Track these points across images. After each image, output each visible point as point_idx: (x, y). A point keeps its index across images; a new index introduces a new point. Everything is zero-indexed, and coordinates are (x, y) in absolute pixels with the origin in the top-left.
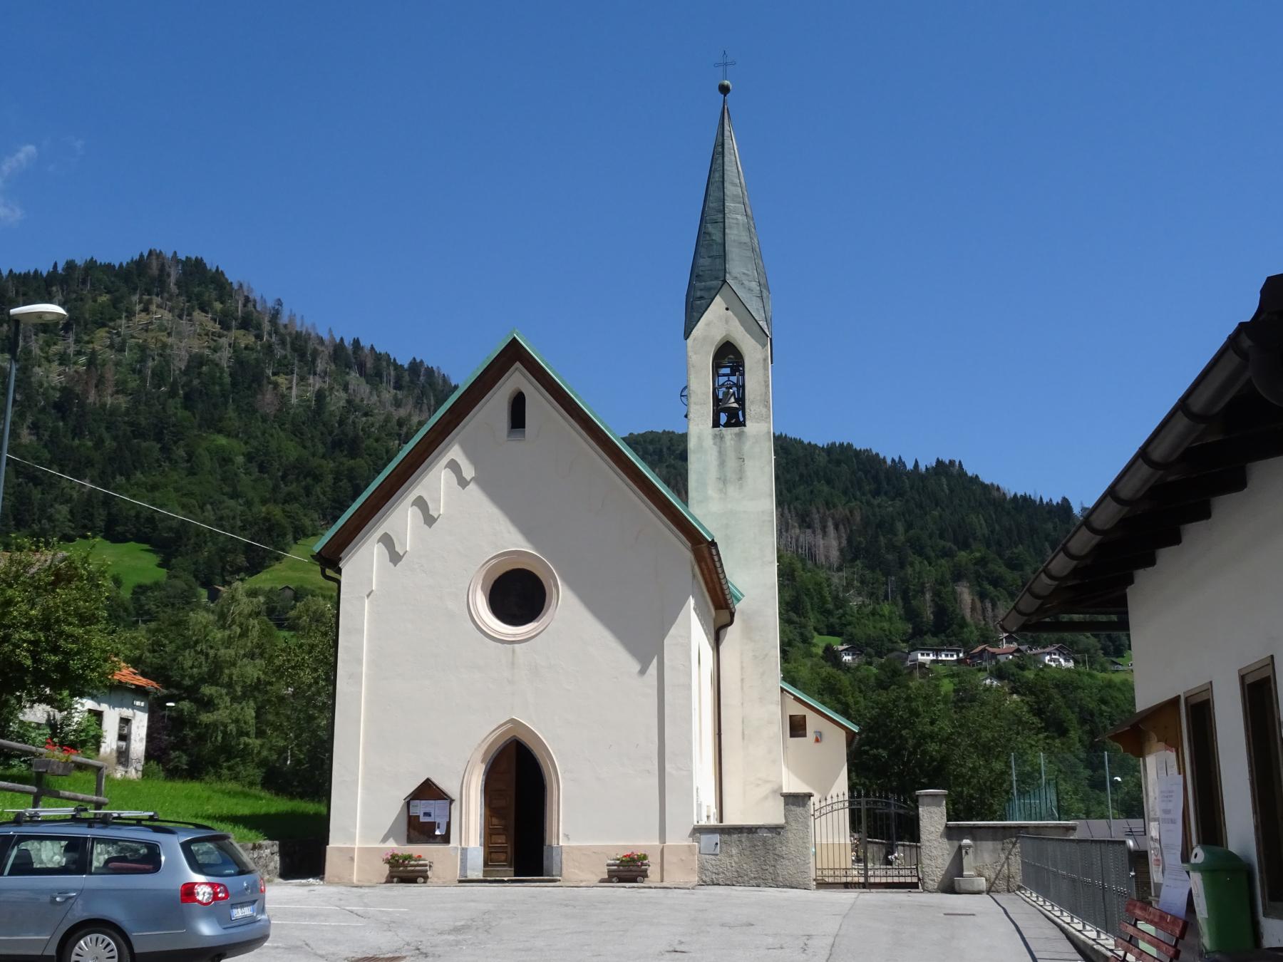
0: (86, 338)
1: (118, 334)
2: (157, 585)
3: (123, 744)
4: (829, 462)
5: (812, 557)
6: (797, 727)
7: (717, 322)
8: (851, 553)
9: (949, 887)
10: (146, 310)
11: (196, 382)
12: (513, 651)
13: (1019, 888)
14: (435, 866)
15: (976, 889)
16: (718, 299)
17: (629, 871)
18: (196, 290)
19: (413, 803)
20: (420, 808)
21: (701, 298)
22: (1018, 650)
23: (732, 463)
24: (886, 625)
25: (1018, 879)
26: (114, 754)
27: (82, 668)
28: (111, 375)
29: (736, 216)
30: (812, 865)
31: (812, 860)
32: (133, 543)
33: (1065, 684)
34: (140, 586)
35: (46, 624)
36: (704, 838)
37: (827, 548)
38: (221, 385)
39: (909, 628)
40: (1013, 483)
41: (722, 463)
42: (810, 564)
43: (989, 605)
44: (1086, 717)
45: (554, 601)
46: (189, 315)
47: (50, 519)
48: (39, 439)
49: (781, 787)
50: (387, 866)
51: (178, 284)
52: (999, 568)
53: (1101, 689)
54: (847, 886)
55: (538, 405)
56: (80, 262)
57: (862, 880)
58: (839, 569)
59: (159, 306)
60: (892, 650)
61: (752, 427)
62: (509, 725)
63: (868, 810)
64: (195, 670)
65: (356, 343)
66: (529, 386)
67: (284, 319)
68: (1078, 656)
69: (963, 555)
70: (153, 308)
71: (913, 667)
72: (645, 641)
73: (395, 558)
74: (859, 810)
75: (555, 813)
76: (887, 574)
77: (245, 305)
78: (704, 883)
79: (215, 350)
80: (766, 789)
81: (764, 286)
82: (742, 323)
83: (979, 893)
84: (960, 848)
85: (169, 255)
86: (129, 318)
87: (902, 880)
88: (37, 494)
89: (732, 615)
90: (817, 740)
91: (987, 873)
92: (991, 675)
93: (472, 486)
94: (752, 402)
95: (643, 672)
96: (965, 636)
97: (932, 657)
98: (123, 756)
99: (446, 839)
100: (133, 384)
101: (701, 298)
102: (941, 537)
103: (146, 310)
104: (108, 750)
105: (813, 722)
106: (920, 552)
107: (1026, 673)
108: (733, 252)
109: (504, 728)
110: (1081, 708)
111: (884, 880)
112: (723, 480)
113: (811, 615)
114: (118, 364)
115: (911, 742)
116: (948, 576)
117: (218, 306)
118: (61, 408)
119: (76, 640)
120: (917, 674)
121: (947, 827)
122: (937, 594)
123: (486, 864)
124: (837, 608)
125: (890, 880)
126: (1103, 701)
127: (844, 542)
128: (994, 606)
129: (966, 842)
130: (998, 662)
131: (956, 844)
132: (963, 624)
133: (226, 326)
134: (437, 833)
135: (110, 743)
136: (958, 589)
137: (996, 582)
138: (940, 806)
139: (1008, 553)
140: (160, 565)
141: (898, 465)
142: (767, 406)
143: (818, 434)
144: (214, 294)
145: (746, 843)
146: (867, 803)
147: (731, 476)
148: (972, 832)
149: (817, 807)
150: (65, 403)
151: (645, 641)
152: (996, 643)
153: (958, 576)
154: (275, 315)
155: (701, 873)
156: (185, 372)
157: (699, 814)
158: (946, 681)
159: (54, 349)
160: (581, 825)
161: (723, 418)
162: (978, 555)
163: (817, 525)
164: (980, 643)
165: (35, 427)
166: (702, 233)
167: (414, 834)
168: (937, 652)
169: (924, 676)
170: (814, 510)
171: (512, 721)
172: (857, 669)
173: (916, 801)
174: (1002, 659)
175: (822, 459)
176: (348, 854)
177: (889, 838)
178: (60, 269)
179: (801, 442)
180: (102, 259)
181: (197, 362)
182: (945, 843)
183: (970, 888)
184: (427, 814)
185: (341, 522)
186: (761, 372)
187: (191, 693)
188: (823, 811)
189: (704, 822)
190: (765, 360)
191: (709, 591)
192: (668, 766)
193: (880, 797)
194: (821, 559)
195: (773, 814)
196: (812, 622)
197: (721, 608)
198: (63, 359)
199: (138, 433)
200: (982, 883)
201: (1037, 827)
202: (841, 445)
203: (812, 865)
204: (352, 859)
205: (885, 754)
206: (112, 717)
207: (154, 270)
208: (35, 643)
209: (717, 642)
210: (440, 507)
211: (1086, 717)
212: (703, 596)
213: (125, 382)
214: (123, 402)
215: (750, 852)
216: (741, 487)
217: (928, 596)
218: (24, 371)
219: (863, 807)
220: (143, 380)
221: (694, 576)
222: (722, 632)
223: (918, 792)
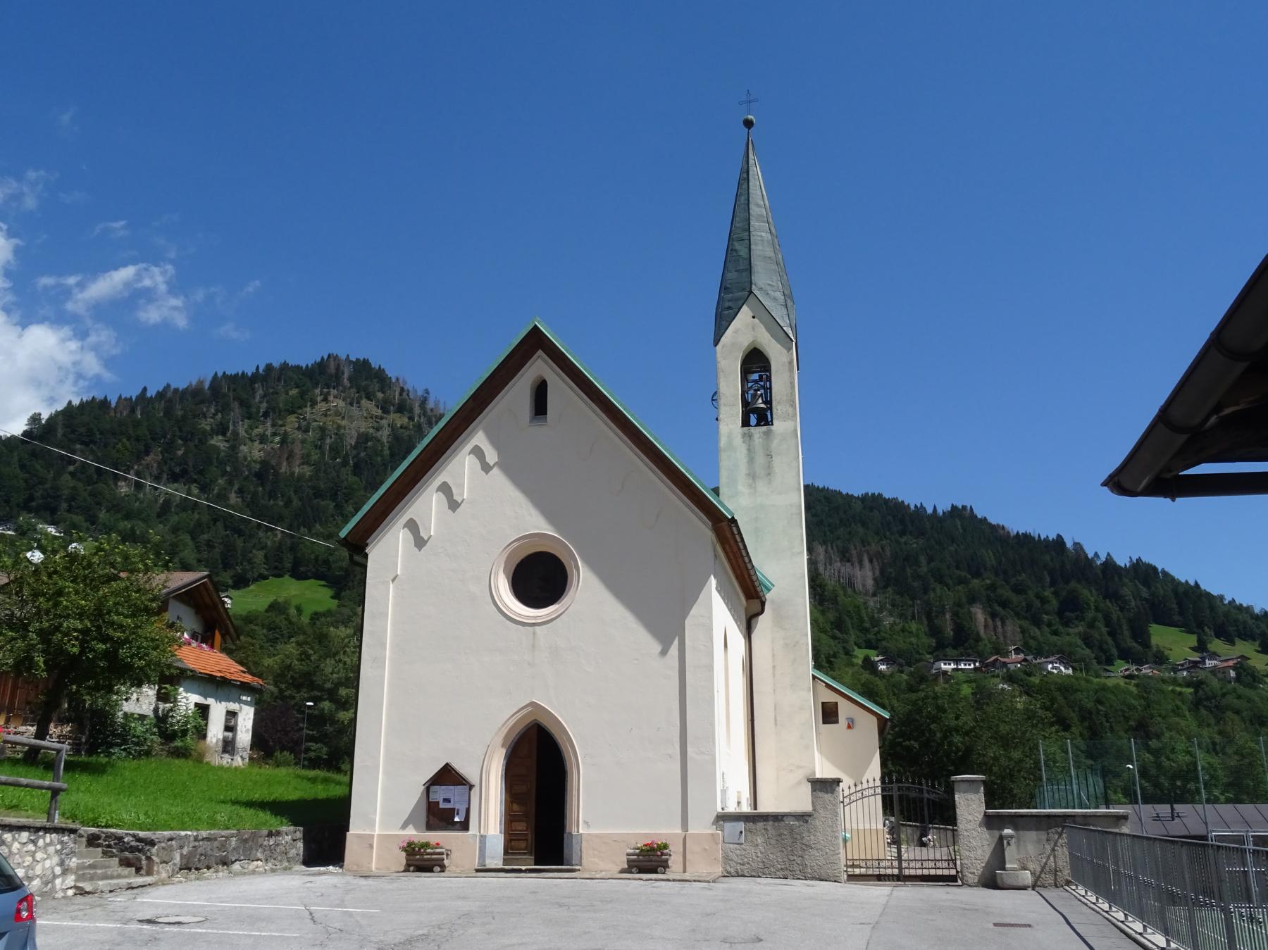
0: (280, 422)
1: (304, 419)
2: (329, 613)
3: (230, 734)
4: (864, 508)
5: (852, 585)
6: (829, 714)
7: (744, 330)
8: (884, 581)
9: (991, 882)
10: (325, 400)
11: (362, 454)
12: (534, 633)
13: (1068, 883)
14: (453, 856)
15: (1021, 884)
16: (745, 308)
17: (649, 860)
18: (364, 383)
19: (433, 788)
20: (440, 793)
21: (729, 308)
22: (1025, 660)
23: (760, 459)
24: (914, 640)
25: (1066, 873)
26: (220, 744)
27: (132, 657)
28: (298, 449)
29: (761, 234)
30: (842, 856)
31: (842, 851)
32: (312, 581)
33: (1065, 688)
34: (316, 614)
35: (99, 612)
36: (728, 826)
38: (382, 456)
39: (933, 642)
41: (751, 460)
43: (999, 623)
44: (1086, 715)
45: (575, 583)
46: (358, 403)
47: (250, 562)
48: (243, 500)
49: (814, 773)
50: (404, 854)
51: (350, 379)
52: (1006, 593)
53: (1096, 691)
54: (880, 878)
55: (561, 392)
56: (276, 365)
57: (896, 872)
58: (874, 595)
59: (335, 397)
60: (918, 661)
61: (779, 425)
62: (530, 709)
63: (900, 796)
64: (335, 676)
67: (430, 405)
69: (976, 582)
70: (331, 398)
71: (937, 675)
72: (667, 621)
73: (420, 543)
74: (891, 797)
75: (575, 799)
76: (913, 598)
77: (401, 394)
78: (728, 875)
79: (378, 430)
80: (800, 775)
81: (789, 296)
82: (768, 329)
83: (1024, 888)
84: (1001, 838)
85: (343, 357)
86: (312, 406)
87: (939, 872)
88: (239, 543)
89: (763, 604)
90: (849, 727)
91: (1031, 866)
93: (496, 471)
95: (664, 652)
96: (980, 648)
97: (953, 666)
98: (228, 746)
99: (465, 826)
100: (315, 457)
101: (729, 308)
102: (958, 568)
103: (325, 400)
104: (214, 741)
105: (845, 709)
106: (940, 579)
107: (1032, 679)
108: (758, 265)
110: (1081, 709)
111: (919, 872)
112: (752, 476)
113: (851, 632)
114: (303, 442)
115: (938, 735)
116: (964, 600)
117: (380, 395)
118: (261, 476)
119: (121, 627)
120: (941, 680)
121: (986, 815)
122: (955, 614)
123: (506, 852)
125: (926, 872)
126: (1099, 701)
127: (877, 573)
128: (1003, 623)
129: (1007, 831)
130: (1008, 670)
131: (996, 833)
132: (978, 639)
133: (385, 411)
134: (457, 819)
135: (215, 731)
136: (973, 610)
137: (1005, 604)
138: (977, 792)
139: (1013, 581)
140: (333, 597)
141: (920, 510)
142: (793, 406)
143: (854, 484)
144: (377, 387)
145: (772, 832)
146: (899, 789)
147: (760, 471)
148: (1014, 821)
149: (846, 793)
150: (264, 473)
151: (667, 621)
152: (1006, 654)
153: (972, 600)
154: (424, 401)
156: (355, 447)
157: (724, 800)
158: (965, 686)
159: (256, 431)
160: (600, 813)
161: (753, 420)
162: (988, 582)
163: (855, 559)
164: (993, 654)
165: (240, 492)
166: (730, 250)
168: (957, 662)
169: (947, 682)
170: (852, 547)
171: (533, 704)
172: (891, 675)
173: (950, 790)
174: (1012, 667)
175: (858, 507)
176: (367, 841)
177: (922, 821)
178: (261, 371)
179: (840, 493)
180: (292, 362)
181: (364, 439)
183: (1015, 884)
184: (447, 800)
185: (366, 508)
187: (332, 695)
188: (853, 798)
189: (732, 808)
190: (791, 363)
191: (737, 578)
193: (913, 783)
194: (859, 587)
195: (801, 801)
196: (852, 638)
197: (750, 597)
198: (263, 439)
199: (318, 494)
200: (1027, 877)
201: (1084, 816)
202: (873, 495)
203: (842, 856)
204: (371, 846)
205: (916, 745)
206: (218, 711)
207: (332, 368)
208: (85, 632)
209: (748, 630)
210: (463, 492)
211: (1086, 715)
212: (726, 572)
213: (309, 455)
214: (307, 471)
215: (777, 841)
216: (770, 482)
217: (948, 616)
218: (234, 448)
219: (896, 794)
220: (323, 454)
221: (716, 556)
222: (753, 621)
223: (953, 778)
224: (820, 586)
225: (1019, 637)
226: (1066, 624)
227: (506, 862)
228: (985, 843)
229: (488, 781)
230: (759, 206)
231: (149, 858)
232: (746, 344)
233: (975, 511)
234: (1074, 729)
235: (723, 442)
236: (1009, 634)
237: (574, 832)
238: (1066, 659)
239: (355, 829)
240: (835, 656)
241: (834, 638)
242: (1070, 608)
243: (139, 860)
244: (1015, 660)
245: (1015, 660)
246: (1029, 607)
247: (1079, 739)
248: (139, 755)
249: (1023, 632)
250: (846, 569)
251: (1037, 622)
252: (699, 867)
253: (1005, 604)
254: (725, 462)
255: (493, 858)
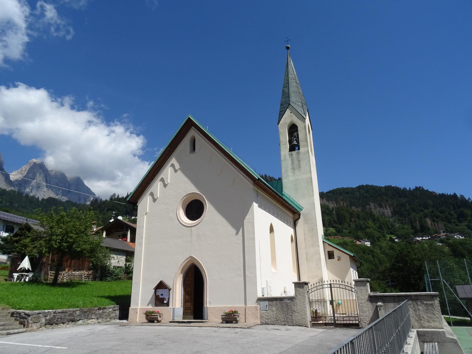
5: (384, 215)
6: (330, 255)
8: (395, 213)
12: (191, 230)
16: (288, 110)
19: (158, 290)
20: (160, 292)
21: (282, 111)
22: (446, 235)
23: (296, 163)
24: (406, 231)
33: (462, 243)
36: (262, 303)
37: (387, 212)
40: (439, 191)
41: (293, 163)
42: (383, 217)
43: (436, 223)
52: (438, 213)
57: (333, 322)
58: (392, 217)
60: (409, 237)
65: (266, 175)
66: (196, 133)
68: (466, 235)
69: (426, 211)
84: (377, 307)
89: (299, 215)
90: (338, 260)
92: (439, 242)
93: (179, 171)
94: (302, 142)
95: (237, 233)
97: (421, 238)
99: (168, 305)
102: (419, 206)
105: (336, 253)
106: (414, 211)
107: (450, 241)
109: (188, 260)
111: (342, 322)
112: (293, 169)
119: (71, 237)
120: (417, 243)
122: (420, 221)
123: (184, 315)
124: (392, 227)
127: (392, 210)
129: (380, 303)
131: (375, 304)
132: (429, 229)
134: (165, 302)
137: (437, 217)
141: (405, 189)
145: (279, 305)
148: (383, 299)
152: (440, 233)
153: (426, 216)
155: (261, 318)
167: (158, 302)
168: (422, 237)
171: (191, 257)
179: (377, 186)
182: (369, 305)
184: (162, 295)
186: (304, 131)
188: (313, 290)
192: (246, 272)
196: (385, 232)
197: (291, 213)
204: (137, 313)
205: (401, 265)
217: (418, 222)
222: (296, 222)
224: (373, 216)
225: (444, 227)
226: (461, 222)
227: (184, 318)
228: (370, 309)
229: (176, 287)
230: (292, 74)
231: (28, 321)
232: (289, 122)
233: (424, 188)
234: (466, 257)
235: (282, 158)
236: (440, 227)
237: (205, 307)
238: (461, 233)
239: (132, 307)
240: (380, 237)
241: (379, 232)
242: (461, 217)
243: (25, 322)
244: (443, 235)
245: (443, 235)
246: (446, 217)
247: (469, 260)
248: (116, 280)
249: (445, 226)
250: (381, 210)
251: (450, 222)
252: (251, 321)
253: (437, 217)
254: (283, 165)
255: (178, 317)
